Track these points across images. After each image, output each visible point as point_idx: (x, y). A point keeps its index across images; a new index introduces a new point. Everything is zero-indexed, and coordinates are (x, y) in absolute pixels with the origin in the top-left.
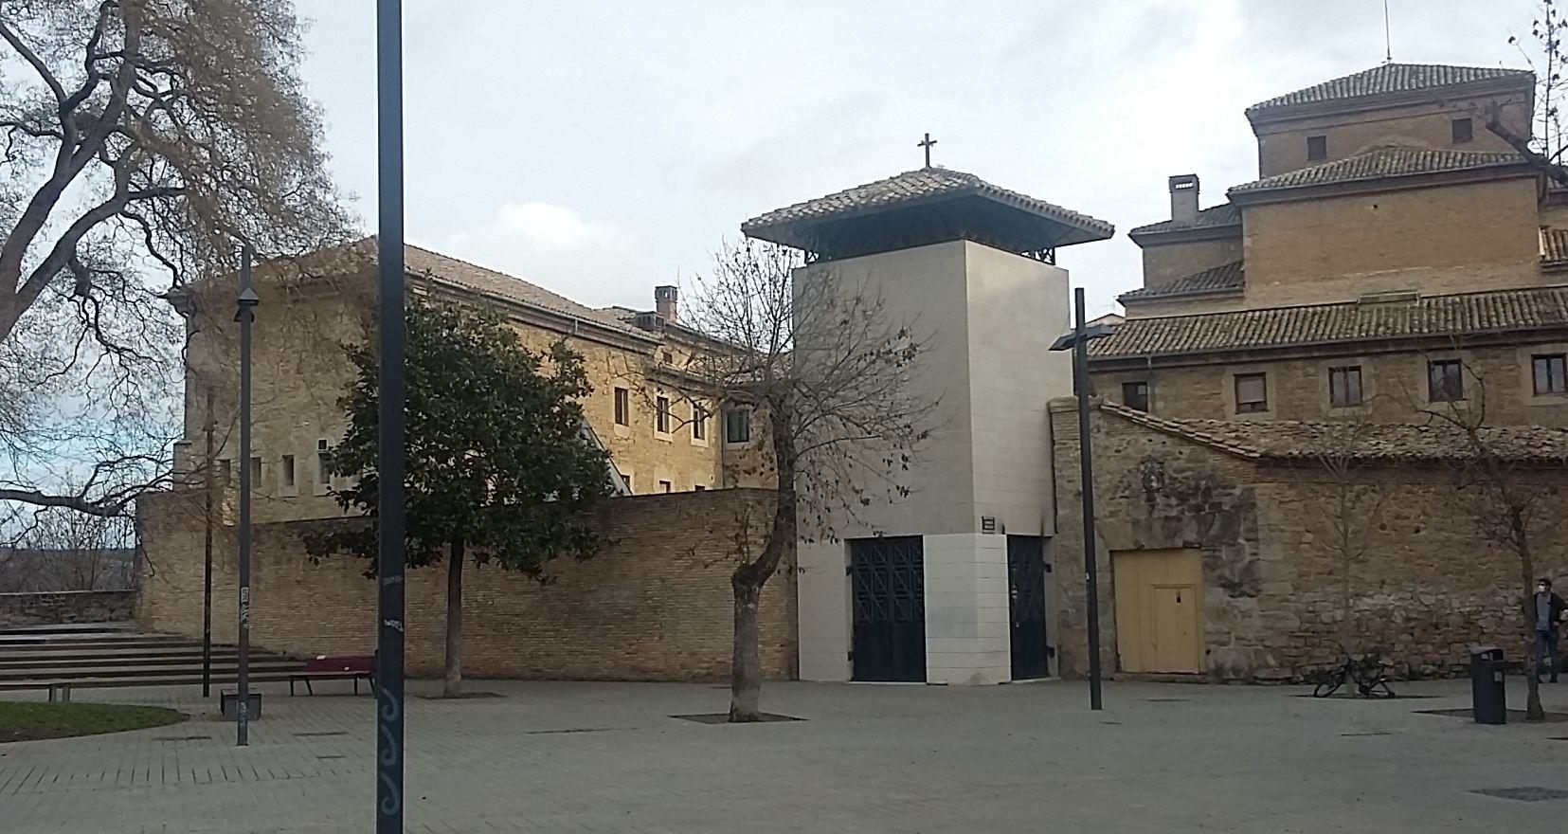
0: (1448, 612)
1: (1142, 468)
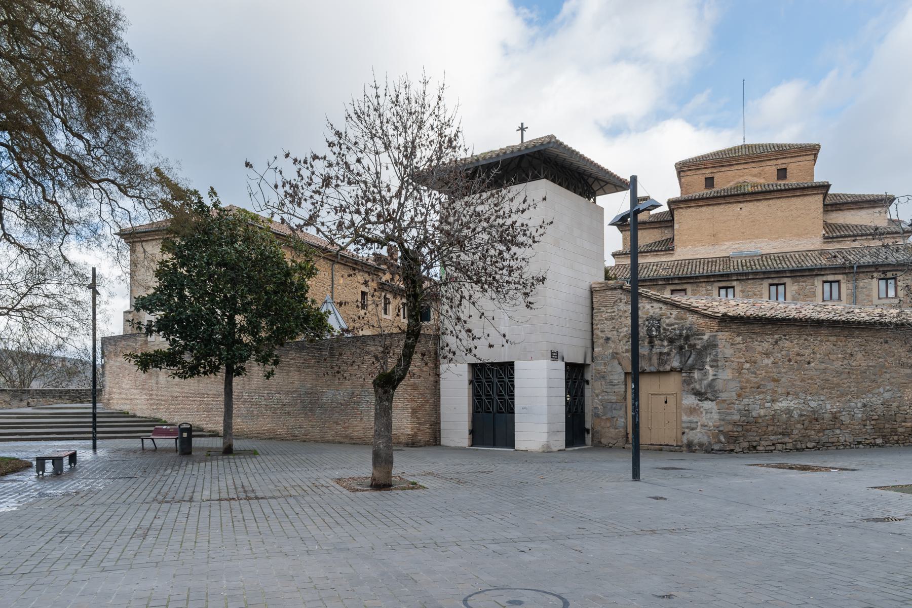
0: (824, 411)
1: (647, 323)
